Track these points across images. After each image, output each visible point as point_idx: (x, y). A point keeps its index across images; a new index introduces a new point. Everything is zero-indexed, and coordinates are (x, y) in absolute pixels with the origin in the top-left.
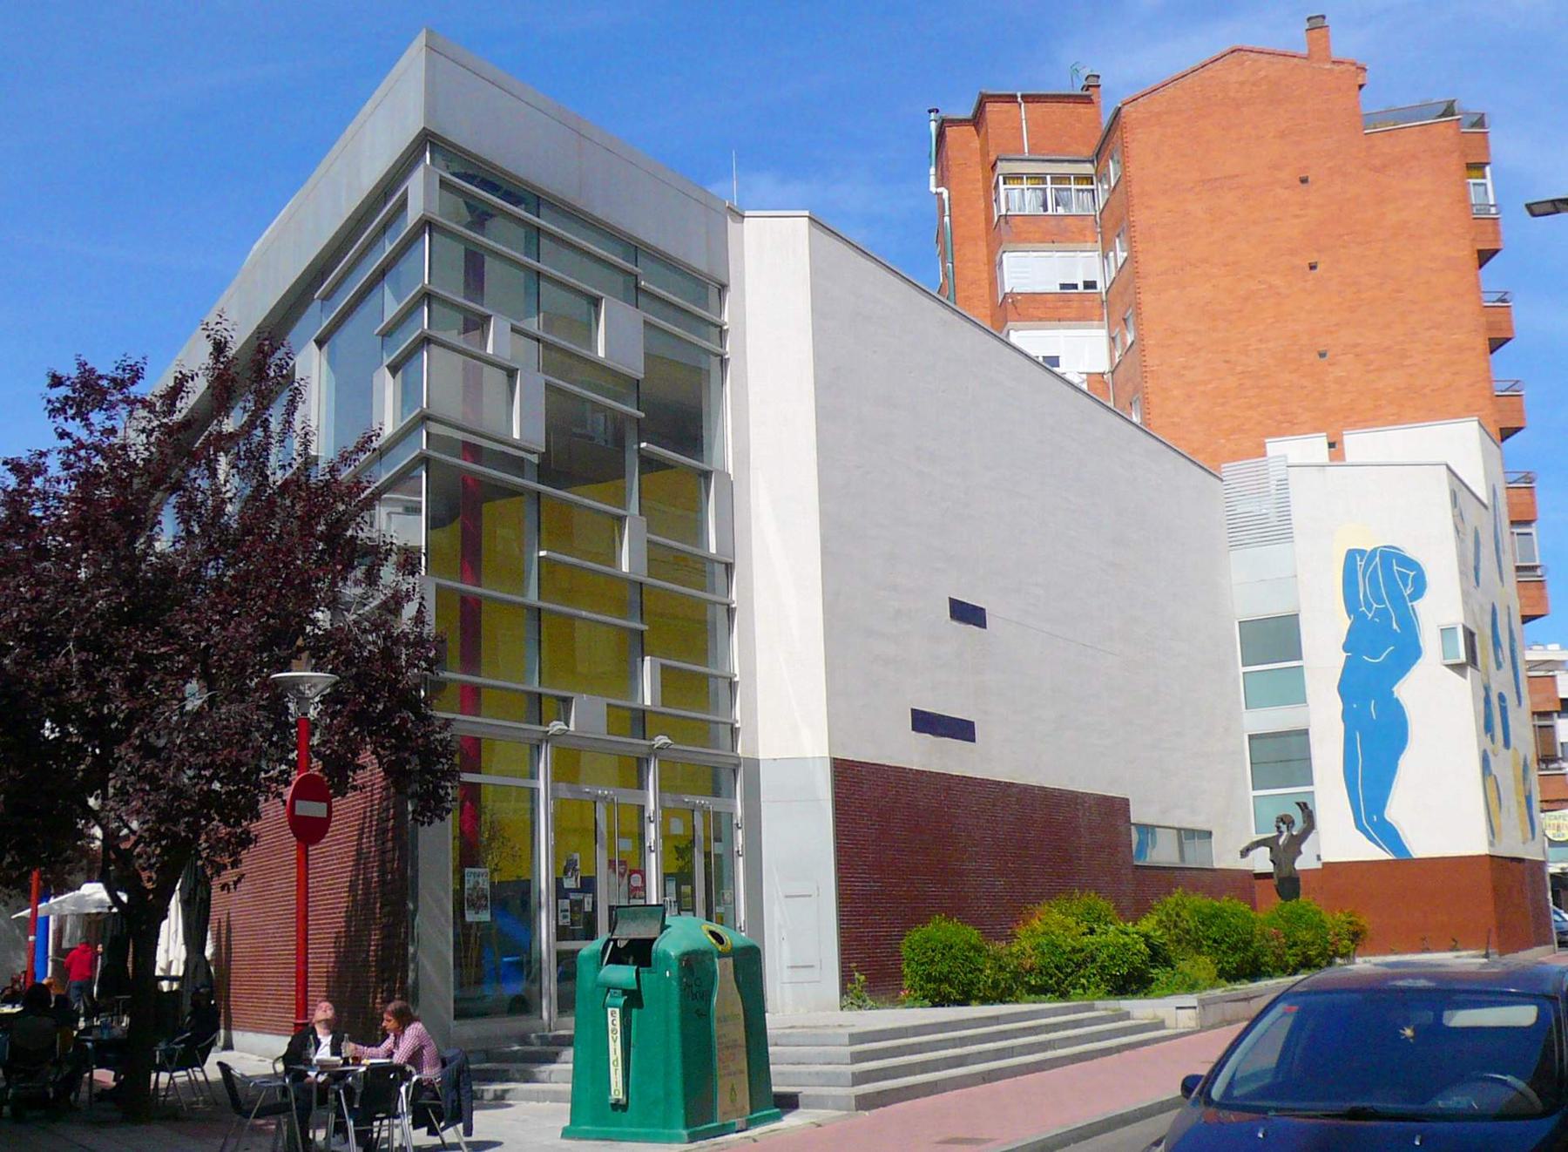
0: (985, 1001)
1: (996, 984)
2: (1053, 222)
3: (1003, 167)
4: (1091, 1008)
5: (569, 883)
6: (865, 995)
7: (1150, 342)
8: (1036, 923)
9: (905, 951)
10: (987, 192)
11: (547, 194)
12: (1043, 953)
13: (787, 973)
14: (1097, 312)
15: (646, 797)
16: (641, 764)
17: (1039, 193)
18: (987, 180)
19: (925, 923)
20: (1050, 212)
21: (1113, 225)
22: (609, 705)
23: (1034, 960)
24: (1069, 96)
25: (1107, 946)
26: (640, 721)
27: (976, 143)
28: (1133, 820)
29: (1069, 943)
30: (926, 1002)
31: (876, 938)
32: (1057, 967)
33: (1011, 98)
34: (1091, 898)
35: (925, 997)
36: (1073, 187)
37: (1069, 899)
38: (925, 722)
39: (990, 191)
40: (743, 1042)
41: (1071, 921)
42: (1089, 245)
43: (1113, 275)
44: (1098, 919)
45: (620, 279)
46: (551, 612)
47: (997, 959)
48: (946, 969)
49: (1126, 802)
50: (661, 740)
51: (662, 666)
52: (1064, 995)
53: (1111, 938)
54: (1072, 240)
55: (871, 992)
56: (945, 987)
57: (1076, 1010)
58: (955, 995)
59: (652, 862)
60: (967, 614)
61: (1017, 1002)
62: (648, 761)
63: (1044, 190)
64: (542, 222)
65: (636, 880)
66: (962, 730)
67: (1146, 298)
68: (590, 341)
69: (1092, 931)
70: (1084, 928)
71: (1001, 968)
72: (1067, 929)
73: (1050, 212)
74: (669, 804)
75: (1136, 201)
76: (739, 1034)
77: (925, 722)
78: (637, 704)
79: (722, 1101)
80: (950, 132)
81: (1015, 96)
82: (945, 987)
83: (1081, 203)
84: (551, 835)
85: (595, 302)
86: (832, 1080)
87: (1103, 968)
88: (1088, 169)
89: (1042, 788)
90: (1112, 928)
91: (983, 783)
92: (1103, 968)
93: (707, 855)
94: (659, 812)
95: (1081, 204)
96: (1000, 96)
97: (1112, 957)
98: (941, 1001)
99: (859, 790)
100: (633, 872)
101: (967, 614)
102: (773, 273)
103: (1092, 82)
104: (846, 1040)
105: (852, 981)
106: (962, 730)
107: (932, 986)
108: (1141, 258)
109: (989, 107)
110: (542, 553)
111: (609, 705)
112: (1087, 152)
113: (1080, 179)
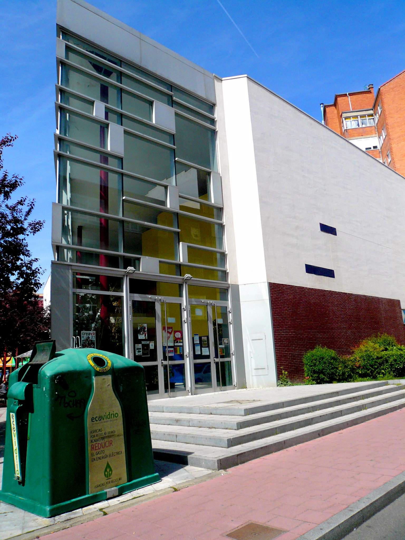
0: (339, 381)
1: (344, 374)
2: (361, 130)
3: (344, 115)
4: (386, 384)
5: (141, 337)
6: (288, 380)
7: (395, 160)
8: (362, 347)
9: (305, 361)
10: (340, 124)
11: (124, 59)
12: (364, 360)
13: (254, 371)
14: (378, 155)
15: (182, 300)
16: (181, 286)
17: (356, 121)
18: (340, 121)
19: (313, 348)
20: (360, 127)
21: (381, 127)
22: (160, 262)
23: (362, 363)
24: (363, 92)
25: (393, 356)
26: (179, 268)
27: (336, 111)
28: (402, 308)
29: (375, 355)
30: (314, 382)
31: (294, 356)
32: (370, 365)
33: (345, 95)
34: (385, 336)
35: (313, 380)
36: (367, 118)
37: (376, 336)
38: (311, 269)
39: (341, 123)
40: (122, 432)
41: (377, 346)
42: (374, 135)
43: (382, 142)
44: (389, 344)
45: (165, 98)
46: (128, 222)
47: (344, 362)
48: (321, 368)
49: (399, 301)
50: (187, 276)
51: (188, 247)
52: (375, 378)
53: (394, 352)
54: (368, 134)
55: (291, 379)
56: (322, 376)
57: (379, 385)
58: (326, 379)
59: (186, 328)
60: (328, 230)
61: (354, 381)
62: (182, 285)
63: (358, 120)
64: (122, 69)
65: (178, 335)
66: (329, 273)
67: (394, 146)
68: (150, 119)
69: (386, 350)
70: (382, 348)
71: (346, 367)
72: (375, 349)
73: (360, 127)
74: (194, 303)
75: (387, 116)
76: (118, 426)
77: (311, 269)
78: (177, 262)
79: (95, 477)
80: (327, 109)
81: (346, 94)
82: (322, 376)
83: (369, 123)
84: (130, 317)
85: (151, 103)
86: (215, 442)
87: (391, 365)
88: (371, 112)
89: (365, 296)
90: (395, 348)
91: (339, 294)
92: (391, 365)
93: (214, 324)
94: (189, 307)
95: (370, 123)
96: (342, 95)
97: (395, 360)
98: (320, 381)
99: (280, 296)
100: (175, 332)
101: (328, 230)
102: (236, 103)
103: (371, 86)
104: (243, 413)
105: (282, 374)
106: (329, 273)
107: (316, 375)
108: (391, 134)
109: (339, 99)
110: (124, 198)
111: (160, 262)
112: (371, 107)
113: (369, 115)
